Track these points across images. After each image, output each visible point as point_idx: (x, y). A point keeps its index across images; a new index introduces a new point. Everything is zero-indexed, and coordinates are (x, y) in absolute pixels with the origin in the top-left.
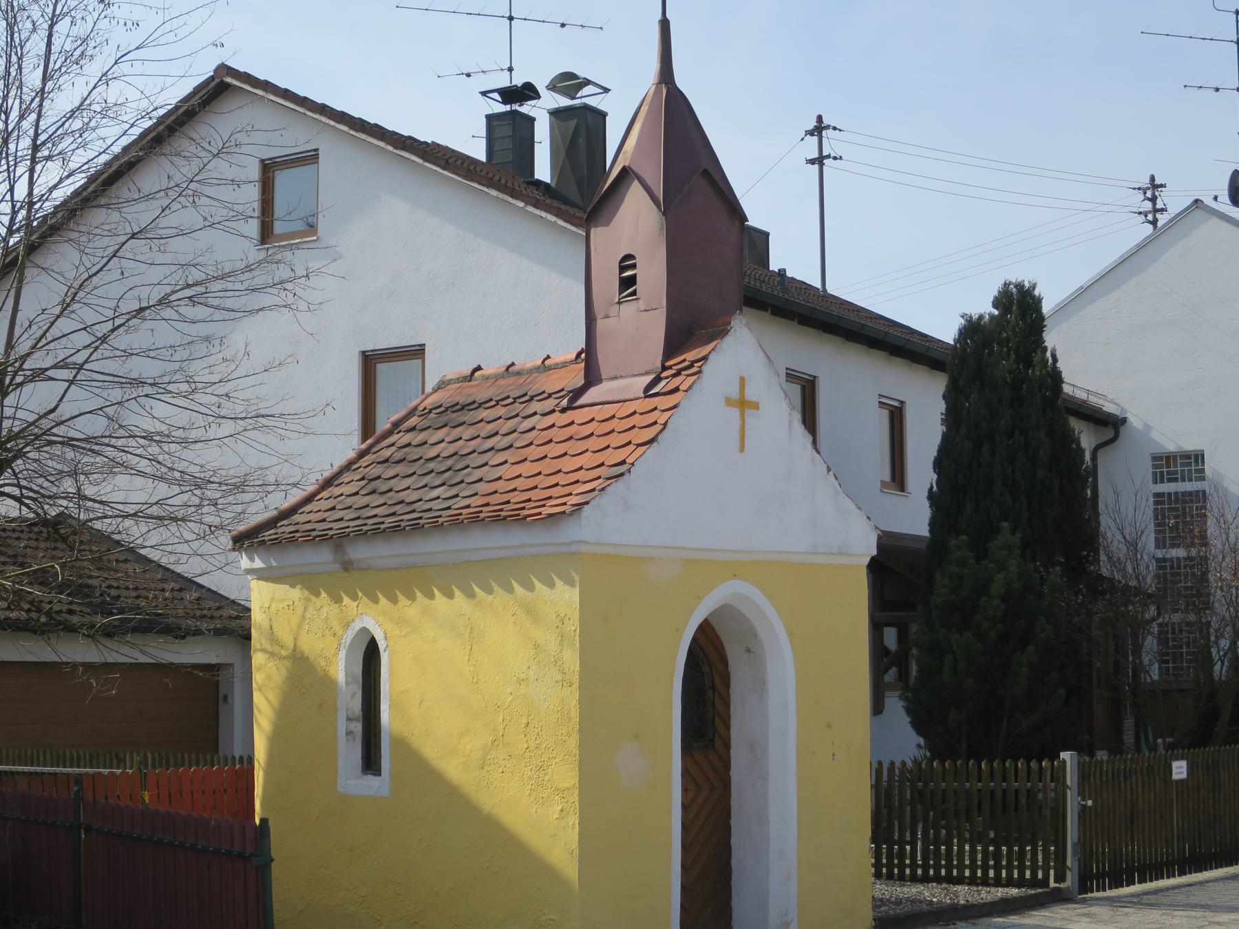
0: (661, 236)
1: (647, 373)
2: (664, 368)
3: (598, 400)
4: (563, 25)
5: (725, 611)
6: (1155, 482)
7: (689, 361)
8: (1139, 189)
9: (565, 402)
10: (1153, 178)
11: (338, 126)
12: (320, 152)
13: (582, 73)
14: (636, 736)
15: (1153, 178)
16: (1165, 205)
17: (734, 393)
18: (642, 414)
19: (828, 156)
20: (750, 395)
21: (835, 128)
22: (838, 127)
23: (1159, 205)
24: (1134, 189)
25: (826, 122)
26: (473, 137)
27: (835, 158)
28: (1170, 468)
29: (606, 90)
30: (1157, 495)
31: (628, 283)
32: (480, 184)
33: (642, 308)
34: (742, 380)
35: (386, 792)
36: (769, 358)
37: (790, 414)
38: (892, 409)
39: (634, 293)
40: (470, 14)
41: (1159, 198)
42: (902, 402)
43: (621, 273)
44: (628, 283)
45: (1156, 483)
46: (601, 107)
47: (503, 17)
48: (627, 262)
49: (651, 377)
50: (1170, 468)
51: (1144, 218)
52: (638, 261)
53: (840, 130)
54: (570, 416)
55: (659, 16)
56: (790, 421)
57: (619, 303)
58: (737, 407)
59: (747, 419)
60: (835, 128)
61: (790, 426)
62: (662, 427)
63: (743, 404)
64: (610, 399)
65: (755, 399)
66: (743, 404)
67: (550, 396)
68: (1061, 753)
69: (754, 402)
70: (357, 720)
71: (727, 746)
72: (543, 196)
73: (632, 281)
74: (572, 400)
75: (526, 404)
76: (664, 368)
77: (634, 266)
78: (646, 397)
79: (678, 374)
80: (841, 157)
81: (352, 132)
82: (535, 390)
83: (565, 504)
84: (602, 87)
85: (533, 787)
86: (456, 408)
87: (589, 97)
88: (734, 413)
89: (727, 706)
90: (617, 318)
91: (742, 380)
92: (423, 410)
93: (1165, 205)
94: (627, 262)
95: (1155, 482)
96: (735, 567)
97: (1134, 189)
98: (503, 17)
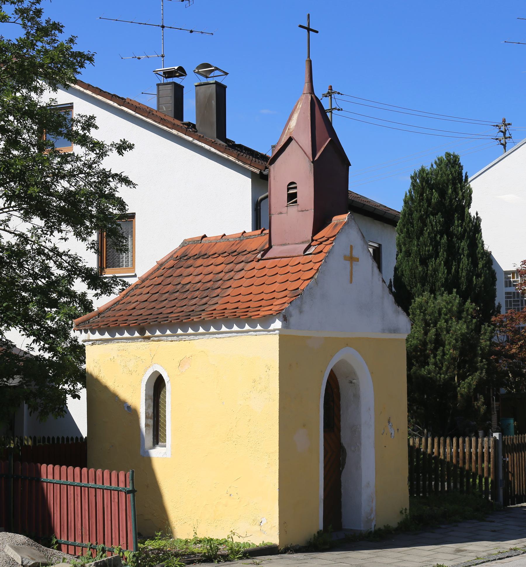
0: (311, 173)
1: (303, 243)
2: (313, 240)
3: (278, 256)
4: (191, 32)
5: (342, 363)
6: (506, 286)
7: (326, 238)
8: (497, 126)
9: (259, 256)
10: (504, 121)
11: (85, 91)
12: (74, 105)
13: (214, 64)
14: (304, 426)
15: (504, 121)
16: (510, 135)
17: (348, 253)
18: (303, 264)
19: (335, 109)
20: (355, 254)
21: (339, 93)
22: (340, 93)
23: (507, 135)
24: (494, 126)
25: (334, 89)
26: (142, 93)
27: (339, 110)
28: (515, 279)
29: (226, 74)
30: (507, 293)
31: (292, 197)
32: (168, 127)
33: (300, 209)
34: (351, 247)
35: (169, 455)
36: (363, 237)
37: (373, 264)
38: (374, 248)
39: (296, 202)
40: (141, 24)
41: (507, 131)
42: (380, 245)
43: (288, 191)
44: (292, 197)
45: (507, 287)
46: (223, 83)
47: (159, 26)
48: (291, 185)
49: (306, 245)
50: (515, 279)
51: (499, 142)
52: (298, 185)
53: (341, 94)
54: (261, 263)
55: (306, 58)
56: (372, 267)
57: (287, 206)
58: (349, 261)
59: (354, 266)
60: (339, 93)
61: (372, 269)
62: (316, 271)
63: (352, 259)
64: (285, 256)
65: (357, 256)
66: (352, 259)
67: (249, 252)
68: (494, 434)
69: (356, 258)
70: (151, 418)
71: (339, 430)
72: (190, 128)
73: (294, 195)
74: (263, 255)
75: (237, 256)
76: (313, 240)
77: (296, 188)
78: (304, 255)
79: (321, 243)
80: (342, 109)
81: (94, 95)
82: (241, 248)
83: (271, 310)
84: (224, 72)
85: (253, 452)
86: (196, 257)
87: (216, 78)
88: (348, 263)
89: (339, 410)
90: (286, 215)
91: (351, 247)
92: (176, 257)
93: (510, 135)
94: (291, 185)
95: (506, 286)
96: (347, 343)
97: (494, 126)
98: (159, 26)
